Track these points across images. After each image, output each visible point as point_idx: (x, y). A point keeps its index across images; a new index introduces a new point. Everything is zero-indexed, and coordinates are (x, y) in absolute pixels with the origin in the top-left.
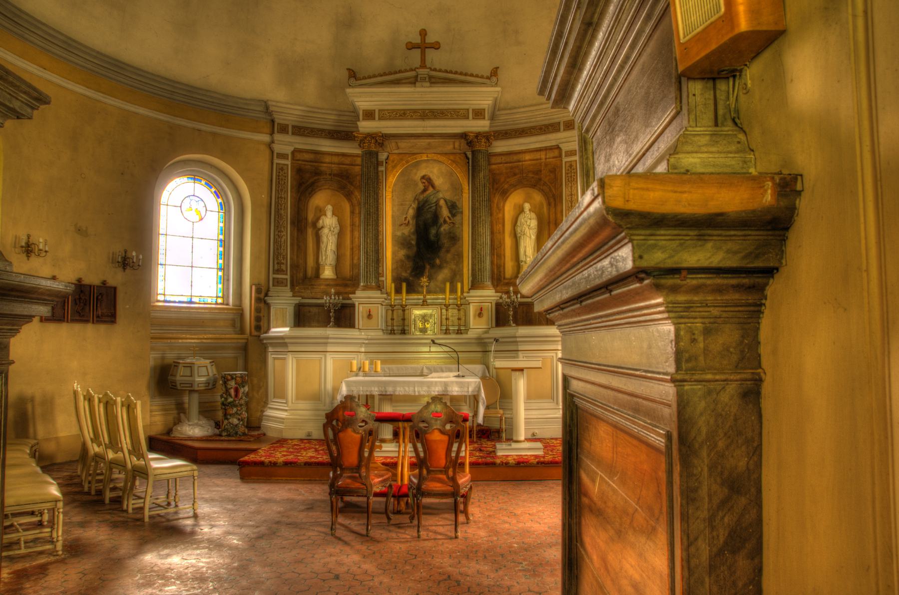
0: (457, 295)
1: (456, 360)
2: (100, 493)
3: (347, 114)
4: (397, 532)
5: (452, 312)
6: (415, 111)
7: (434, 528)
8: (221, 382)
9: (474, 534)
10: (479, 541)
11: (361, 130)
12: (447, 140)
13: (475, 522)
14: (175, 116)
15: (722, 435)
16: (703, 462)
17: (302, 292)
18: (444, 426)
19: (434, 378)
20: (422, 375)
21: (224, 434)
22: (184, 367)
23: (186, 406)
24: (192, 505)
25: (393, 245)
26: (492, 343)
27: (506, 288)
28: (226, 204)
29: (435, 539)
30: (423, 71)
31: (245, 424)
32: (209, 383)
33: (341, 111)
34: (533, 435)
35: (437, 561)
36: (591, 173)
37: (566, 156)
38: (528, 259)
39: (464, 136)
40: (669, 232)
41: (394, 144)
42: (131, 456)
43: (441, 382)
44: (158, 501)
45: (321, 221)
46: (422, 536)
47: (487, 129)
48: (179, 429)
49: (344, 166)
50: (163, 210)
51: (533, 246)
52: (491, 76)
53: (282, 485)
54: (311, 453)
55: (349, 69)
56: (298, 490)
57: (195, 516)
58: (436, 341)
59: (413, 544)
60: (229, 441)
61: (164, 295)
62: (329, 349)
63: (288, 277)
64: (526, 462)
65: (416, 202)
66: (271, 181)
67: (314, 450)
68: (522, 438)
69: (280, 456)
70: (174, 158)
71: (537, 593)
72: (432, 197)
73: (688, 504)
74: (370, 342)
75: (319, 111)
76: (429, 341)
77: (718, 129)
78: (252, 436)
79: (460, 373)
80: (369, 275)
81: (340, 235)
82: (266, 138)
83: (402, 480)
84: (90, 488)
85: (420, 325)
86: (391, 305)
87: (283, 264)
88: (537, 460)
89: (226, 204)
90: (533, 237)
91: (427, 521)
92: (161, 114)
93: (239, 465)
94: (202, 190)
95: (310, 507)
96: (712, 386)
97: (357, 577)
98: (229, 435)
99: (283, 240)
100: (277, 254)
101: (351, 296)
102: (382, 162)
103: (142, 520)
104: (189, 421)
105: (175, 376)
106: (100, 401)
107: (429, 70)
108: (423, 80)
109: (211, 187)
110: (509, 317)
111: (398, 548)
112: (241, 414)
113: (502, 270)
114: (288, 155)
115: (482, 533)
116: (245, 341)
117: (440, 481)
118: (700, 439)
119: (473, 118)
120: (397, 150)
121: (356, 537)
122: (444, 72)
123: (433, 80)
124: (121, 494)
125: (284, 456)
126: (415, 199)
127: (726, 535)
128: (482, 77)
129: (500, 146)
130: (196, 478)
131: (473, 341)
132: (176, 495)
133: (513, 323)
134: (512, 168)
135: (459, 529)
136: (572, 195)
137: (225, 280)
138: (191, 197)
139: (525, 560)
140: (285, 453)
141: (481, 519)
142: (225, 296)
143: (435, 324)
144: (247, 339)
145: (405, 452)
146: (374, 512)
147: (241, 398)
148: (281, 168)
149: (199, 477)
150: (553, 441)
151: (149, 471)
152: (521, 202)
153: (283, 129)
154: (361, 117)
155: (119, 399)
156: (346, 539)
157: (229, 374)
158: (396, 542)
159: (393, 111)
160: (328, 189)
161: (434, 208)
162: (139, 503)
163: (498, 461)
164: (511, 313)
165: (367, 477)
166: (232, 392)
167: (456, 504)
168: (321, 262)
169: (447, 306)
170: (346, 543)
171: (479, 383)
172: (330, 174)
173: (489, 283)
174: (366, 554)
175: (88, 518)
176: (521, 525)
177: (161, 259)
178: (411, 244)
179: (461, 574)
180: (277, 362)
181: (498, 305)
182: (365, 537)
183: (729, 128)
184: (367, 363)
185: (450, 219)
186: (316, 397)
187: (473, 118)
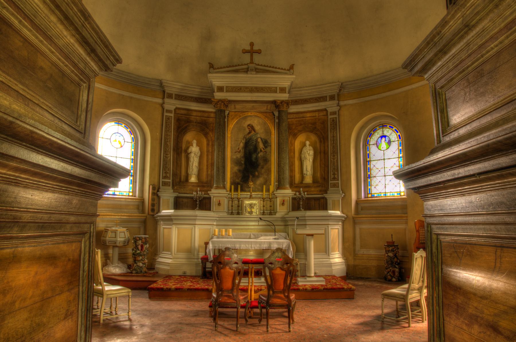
4: (253, 329)
6: (247, 88)
7: (274, 326)
8: (133, 241)
9: (299, 330)
10: (304, 333)
11: (216, 97)
12: (264, 105)
14: (109, 87)
17: (179, 190)
18: (283, 266)
20: (250, 238)
21: (134, 272)
22: (111, 232)
23: (111, 255)
24: (127, 313)
25: (231, 164)
26: (295, 220)
27: (298, 189)
28: (136, 138)
29: (277, 332)
31: (146, 266)
32: (125, 242)
33: (203, 87)
37: (330, 115)
38: (308, 173)
39: (274, 102)
41: (233, 106)
43: (267, 242)
44: (106, 311)
45: (190, 149)
46: (269, 331)
47: (287, 99)
49: (204, 118)
51: (311, 165)
52: (290, 69)
53: (175, 302)
55: (209, 63)
56: (185, 305)
57: (130, 320)
58: (262, 219)
59: (265, 335)
62: (197, 222)
63: (171, 181)
64: (317, 289)
65: (245, 139)
66: (162, 125)
67: (190, 282)
69: (172, 285)
70: (107, 112)
72: (254, 136)
75: (191, 86)
78: (150, 273)
79: (276, 237)
80: (219, 180)
81: (201, 158)
82: (160, 101)
85: (249, 210)
86: (231, 198)
87: (168, 173)
88: (323, 287)
89: (136, 138)
90: (311, 160)
91: (271, 322)
92: (101, 85)
93: (148, 290)
94: (122, 130)
95: (197, 314)
98: (137, 273)
99: (168, 159)
101: (209, 192)
104: (112, 264)
105: (106, 237)
107: (255, 65)
108: (252, 70)
110: (300, 206)
112: (144, 260)
114: (172, 111)
115: (303, 329)
116: (145, 218)
119: (279, 92)
120: (234, 109)
121: (230, 332)
122: (263, 66)
123: (257, 70)
126: (244, 137)
128: (285, 69)
130: (130, 297)
131: (279, 219)
132: (116, 307)
133: (303, 209)
135: (291, 327)
136: (333, 137)
140: (174, 283)
141: (300, 321)
142: (134, 192)
143: (257, 209)
144: (146, 217)
145: (252, 283)
147: (145, 251)
148: (168, 118)
149: (131, 298)
150: (328, 277)
151: (104, 292)
152: (304, 141)
153: (170, 96)
154: (216, 90)
159: (234, 87)
163: (301, 288)
165: (237, 296)
166: (140, 247)
168: (189, 173)
170: (226, 335)
172: (196, 122)
173: (288, 186)
176: (324, 324)
178: (241, 163)
180: (166, 230)
181: (293, 199)
184: (217, 230)
186: (190, 251)
187: (279, 92)
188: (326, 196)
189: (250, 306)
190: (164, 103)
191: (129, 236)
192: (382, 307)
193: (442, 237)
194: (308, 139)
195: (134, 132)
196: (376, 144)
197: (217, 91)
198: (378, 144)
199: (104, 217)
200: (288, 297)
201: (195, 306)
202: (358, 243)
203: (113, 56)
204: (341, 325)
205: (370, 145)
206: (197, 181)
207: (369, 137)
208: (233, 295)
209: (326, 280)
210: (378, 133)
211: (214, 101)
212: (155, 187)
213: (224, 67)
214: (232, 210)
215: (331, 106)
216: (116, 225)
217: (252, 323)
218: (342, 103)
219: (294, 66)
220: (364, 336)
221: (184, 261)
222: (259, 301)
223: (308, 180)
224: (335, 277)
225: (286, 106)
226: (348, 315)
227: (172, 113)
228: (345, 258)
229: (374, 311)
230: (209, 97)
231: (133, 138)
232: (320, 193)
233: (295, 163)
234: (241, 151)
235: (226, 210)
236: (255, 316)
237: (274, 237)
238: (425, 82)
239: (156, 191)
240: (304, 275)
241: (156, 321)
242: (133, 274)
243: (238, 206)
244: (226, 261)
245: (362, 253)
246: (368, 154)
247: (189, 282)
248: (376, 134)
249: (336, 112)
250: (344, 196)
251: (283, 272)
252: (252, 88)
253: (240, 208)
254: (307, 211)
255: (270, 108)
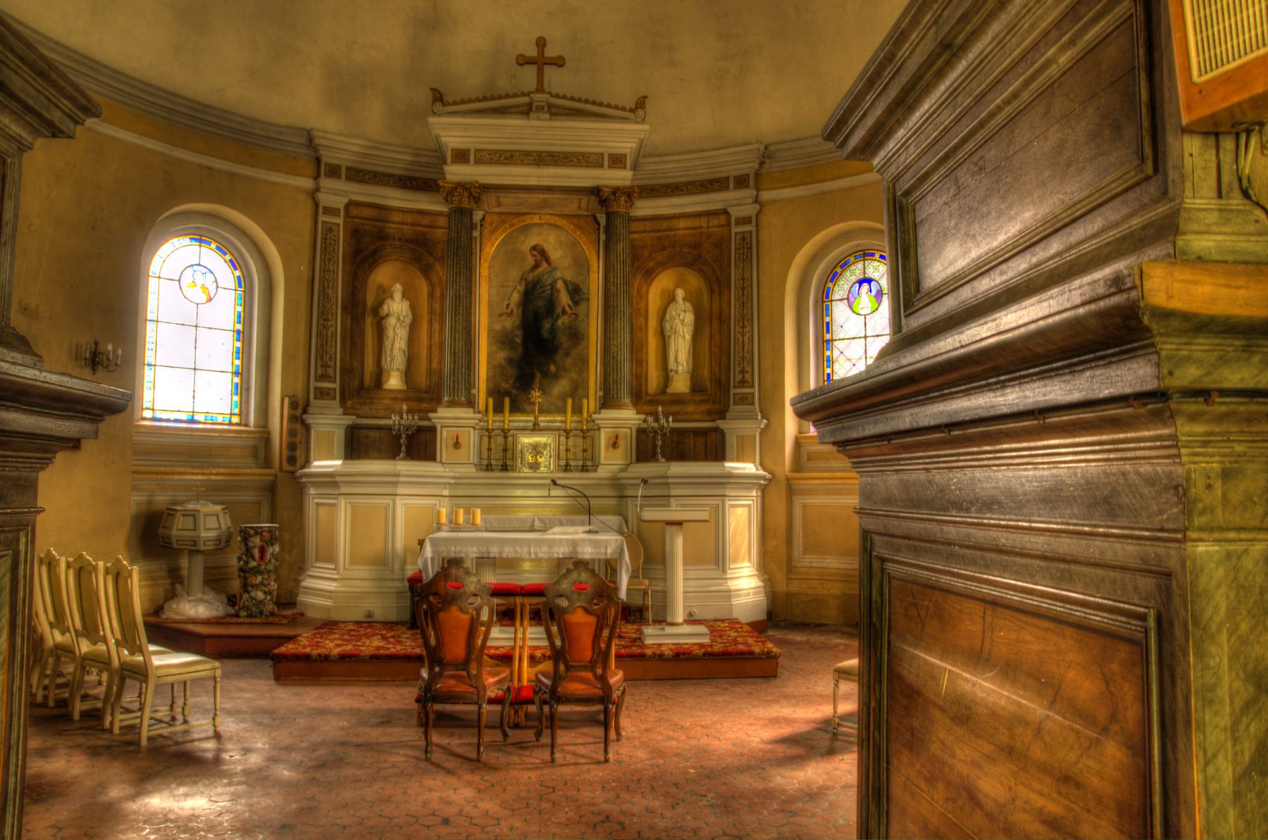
0: (566, 416)
1: (583, 509)
2: (63, 703)
3: (427, 153)
4: (520, 755)
5: (576, 442)
6: (527, 154)
8: (239, 539)
10: (640, 765)
11: (449, 177)
13: (628, 738)
15: (1244, 613)
16: (1222, 650)
19: (557, 533)
20: (532, 530)
21: (243, 613)
23: (185, 572)
25: (490, 344)
29: (576, 764)
30: (540, 98)
34: (690, 615)
35: (586, 795)
36: (912, 251)
37: (737, 224)
38: (680, 368)
39: (596, 191)
40: (1209, 341)
42: (120, 649)
43: (567, 540)
44: (158, 715)
45: (385, 307)
47: (628, 183)
48: (174, 606)
49: (420, 228)
50: (153, 284)
53: (338, 689)
54: (377, 642)
55: (433, 90)
56: (363, 696)
57: (217, 736)
58: (558, 482)
59: (546, 771)
60: (251, 624)
61: (153, 410)
62: (401, 490)
63: (336, 386)
64: (688, 654)
65: (523, 283)
68: (680, 619)
69: (332, 646)
71: (735, 837)
72: (546, 276)
73: (1204, 706)
74: (458, 482)
75: (388, 148)
76: (548, 482)
77: (1223, 202)
78: (285, 617)
79: (591, 527)
81: (413, 328)
82: (308, 183)
83: (520, 680)
84: (46, 697)
85: (530, 459)
86: (488, 430)
87: (330, 366)
88: (703, 650)
90: (688, 337)
91: (563, 737)
93: (273, 659)
94: (211, 257)
95: (387, 719)
96: (1232, 547)
97: (476, 821)
98: (250, 616)
99: (330, 333)
100: (322, 353)
101: (431, 415)
102: (476, 224)
103: (137, 743)
104: (188, 595)
105: (170, 528)
106: (68, 566)
108: (540, 109)
109: (225, 254)
111: (525, 777)
112: (269, 584)
113: (644, 382)
114: (339, 210)
115: (641, 754)
116: (271, 478)
117: (583, 681)
118: (1218, 619)
119: (609, 167)
123: (554, 110)
124: (100, 705)
125: (339, 645)
126: (522, 278)
127: (1253, 750)
128: (624, 109)
129: (645, 208)
131: (605, 482)
134: (659, 239)
135: (610, 750)
136: (743, 279)
137: (242, 390)
138: (195, 268)
139: (710, 791)
140: (338, 642)
141: (636, 735)
142: (243, 413)
144: (276, 476)
145: (524, 639)
146: (487, 727)
147: (270, 561)
148: (329, 229)
151: (149, 670)
152: (671, 287)
153: (334, 172)
154: (449, 160)
155: (101, 564)
156: (447, 765)
157: (252, 528)
158: (522, 769)
159: (496, 151)
160: (397, 260)
161: (549, 292)
162: (129, 719)
163: (649, 652)
164: (660, 443)
165: (479, 676)
166: (256, 553)
167: (606, 711)
168: (385, 365)
169: (567, 433)
170: (449, 772)
171: (622, 541)
172: (400, 240)
173: (627, 400)
174: (482, 787)
175: (49, 743)
176: (693, 742)
177: (149, 357)
179: (624, 813)
180: (322, 510)
181: (641, 432)
182: (476, 763)
183: (1236, 201)
185: (571, 309)
186: (382, 561)
187: (609, 167)
188: (721, 424)
189: (515, 699)
190: (317, 189)
191: (229, 524)
192: (835, 699)
193: (888, 565)
194: (680, 284)
195: (241, 263)
196: (848, 299)
197: (453, 162)
198: (851, 300)
199: (165, 477)
200: (603, 679)
201: (385, 698)
202: (798, 540)
203: (70, 98)
204: (733, 745)
205: (832, 301)
206: (404, 387)
207: (831, 281)
208: (469, 675)
209: (713, 631)
210: (852, 273)
211: (445, 187)
212: (297, 403)
213: (470, 101)
214: (489, 458)
215: (737, 202)
216: (197, 499)
217: (519, 740)
218: (766, 196)
219: (647, 100)
220: (783, 771)
221: (366, 586)
222: (537, 687)
223: (681, 385)
224: (738, 623)
225: (626, 202)
226: (756, 719)
227: (339, 216)
228: (767, 577)
229: (819, 707)
230: (434, 176)
231: (239, 278)
232: (709, 418)
233: (647, 345)
234: (515, 311)
235: (473, 458)
236: (529, 723)
237: (587, 528)
238: (872, 177)
239: (299, 412)
240: (659, 618)
241: (284, 736)
242: (241, 620)
243: (505, 450)
244: (451, 591)
245: (808, 564)
246: (828, 323)
247: (376, 638)
248: (848, 274)
249: (750, 218)
250: (767, 426)
251: (592, 620)
252: (540, 153)
253: (509, 454)
254: (673, 464)
255: (588, 205)
